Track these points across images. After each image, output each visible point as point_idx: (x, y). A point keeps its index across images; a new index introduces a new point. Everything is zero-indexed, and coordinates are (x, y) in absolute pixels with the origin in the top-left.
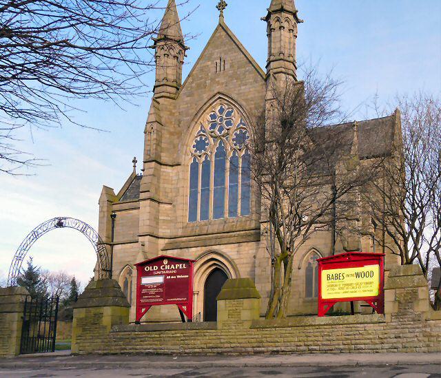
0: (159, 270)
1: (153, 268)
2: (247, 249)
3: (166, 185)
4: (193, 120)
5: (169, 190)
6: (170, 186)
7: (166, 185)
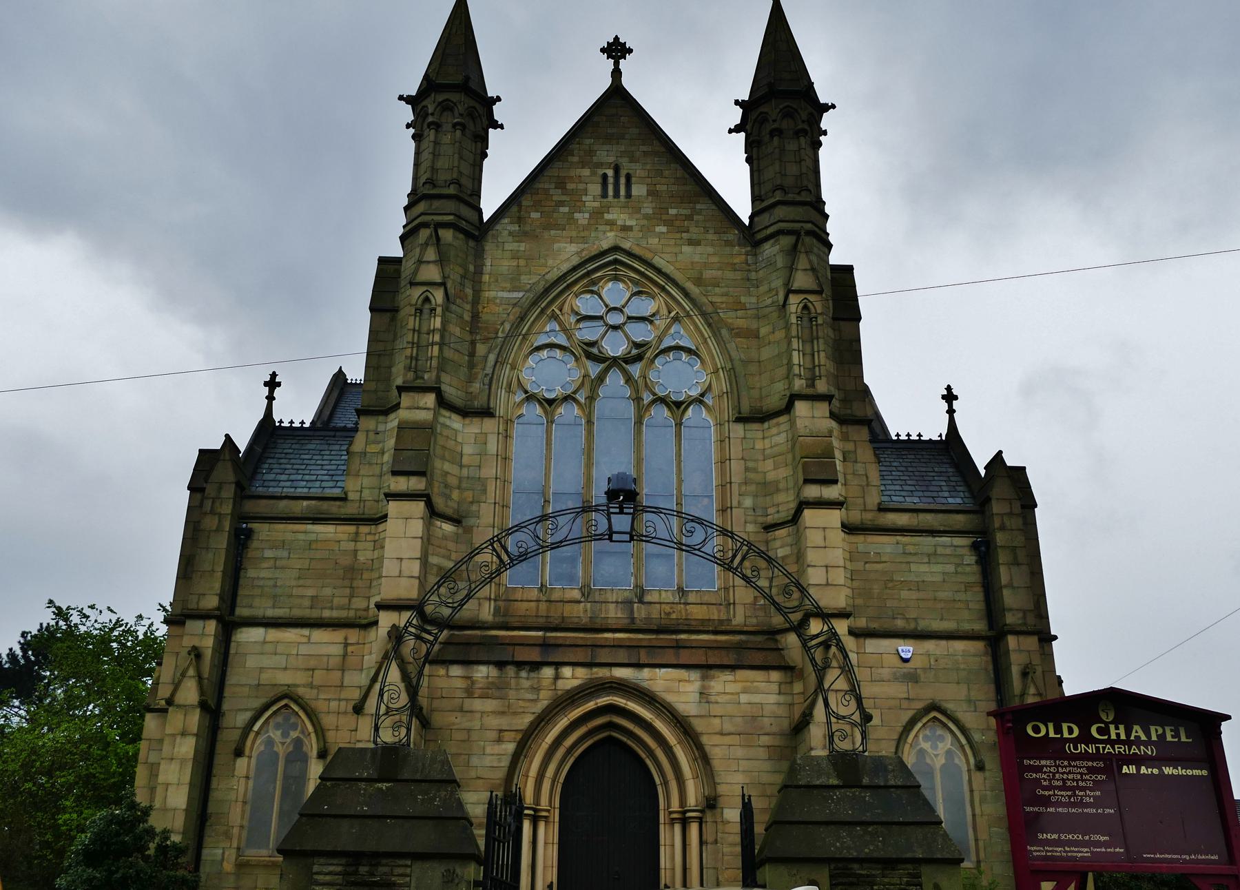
0: (1086, 738)
1: (1058, 730)
2: (731, 688)
3: (447, 466)
4: (534, 303)
5: (453, 481)
6: (453, 469)
7: (447, 466)
